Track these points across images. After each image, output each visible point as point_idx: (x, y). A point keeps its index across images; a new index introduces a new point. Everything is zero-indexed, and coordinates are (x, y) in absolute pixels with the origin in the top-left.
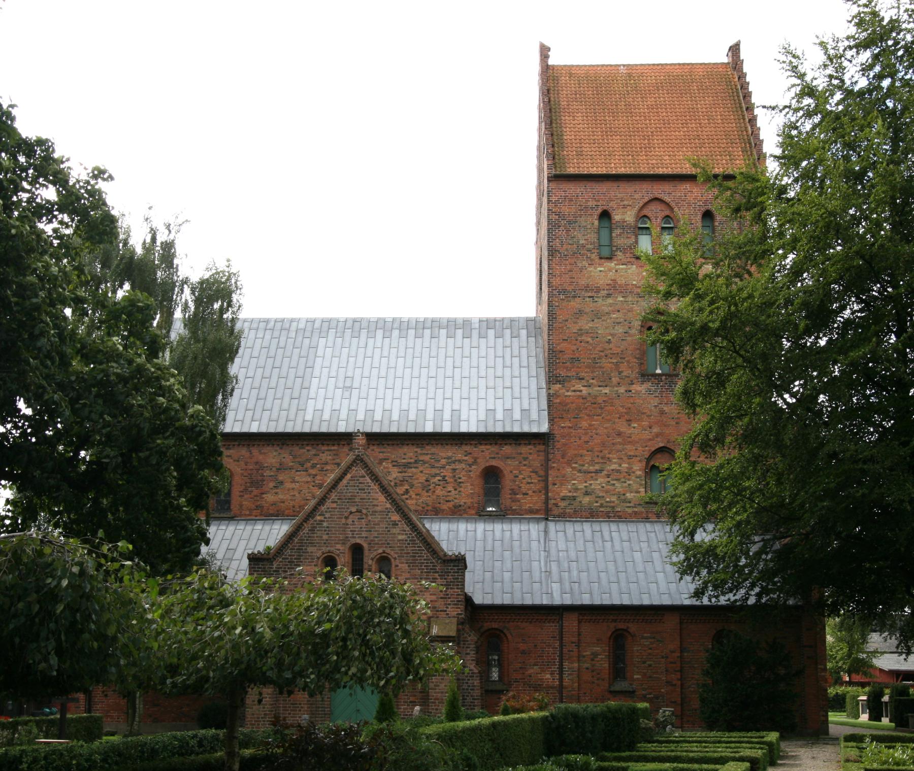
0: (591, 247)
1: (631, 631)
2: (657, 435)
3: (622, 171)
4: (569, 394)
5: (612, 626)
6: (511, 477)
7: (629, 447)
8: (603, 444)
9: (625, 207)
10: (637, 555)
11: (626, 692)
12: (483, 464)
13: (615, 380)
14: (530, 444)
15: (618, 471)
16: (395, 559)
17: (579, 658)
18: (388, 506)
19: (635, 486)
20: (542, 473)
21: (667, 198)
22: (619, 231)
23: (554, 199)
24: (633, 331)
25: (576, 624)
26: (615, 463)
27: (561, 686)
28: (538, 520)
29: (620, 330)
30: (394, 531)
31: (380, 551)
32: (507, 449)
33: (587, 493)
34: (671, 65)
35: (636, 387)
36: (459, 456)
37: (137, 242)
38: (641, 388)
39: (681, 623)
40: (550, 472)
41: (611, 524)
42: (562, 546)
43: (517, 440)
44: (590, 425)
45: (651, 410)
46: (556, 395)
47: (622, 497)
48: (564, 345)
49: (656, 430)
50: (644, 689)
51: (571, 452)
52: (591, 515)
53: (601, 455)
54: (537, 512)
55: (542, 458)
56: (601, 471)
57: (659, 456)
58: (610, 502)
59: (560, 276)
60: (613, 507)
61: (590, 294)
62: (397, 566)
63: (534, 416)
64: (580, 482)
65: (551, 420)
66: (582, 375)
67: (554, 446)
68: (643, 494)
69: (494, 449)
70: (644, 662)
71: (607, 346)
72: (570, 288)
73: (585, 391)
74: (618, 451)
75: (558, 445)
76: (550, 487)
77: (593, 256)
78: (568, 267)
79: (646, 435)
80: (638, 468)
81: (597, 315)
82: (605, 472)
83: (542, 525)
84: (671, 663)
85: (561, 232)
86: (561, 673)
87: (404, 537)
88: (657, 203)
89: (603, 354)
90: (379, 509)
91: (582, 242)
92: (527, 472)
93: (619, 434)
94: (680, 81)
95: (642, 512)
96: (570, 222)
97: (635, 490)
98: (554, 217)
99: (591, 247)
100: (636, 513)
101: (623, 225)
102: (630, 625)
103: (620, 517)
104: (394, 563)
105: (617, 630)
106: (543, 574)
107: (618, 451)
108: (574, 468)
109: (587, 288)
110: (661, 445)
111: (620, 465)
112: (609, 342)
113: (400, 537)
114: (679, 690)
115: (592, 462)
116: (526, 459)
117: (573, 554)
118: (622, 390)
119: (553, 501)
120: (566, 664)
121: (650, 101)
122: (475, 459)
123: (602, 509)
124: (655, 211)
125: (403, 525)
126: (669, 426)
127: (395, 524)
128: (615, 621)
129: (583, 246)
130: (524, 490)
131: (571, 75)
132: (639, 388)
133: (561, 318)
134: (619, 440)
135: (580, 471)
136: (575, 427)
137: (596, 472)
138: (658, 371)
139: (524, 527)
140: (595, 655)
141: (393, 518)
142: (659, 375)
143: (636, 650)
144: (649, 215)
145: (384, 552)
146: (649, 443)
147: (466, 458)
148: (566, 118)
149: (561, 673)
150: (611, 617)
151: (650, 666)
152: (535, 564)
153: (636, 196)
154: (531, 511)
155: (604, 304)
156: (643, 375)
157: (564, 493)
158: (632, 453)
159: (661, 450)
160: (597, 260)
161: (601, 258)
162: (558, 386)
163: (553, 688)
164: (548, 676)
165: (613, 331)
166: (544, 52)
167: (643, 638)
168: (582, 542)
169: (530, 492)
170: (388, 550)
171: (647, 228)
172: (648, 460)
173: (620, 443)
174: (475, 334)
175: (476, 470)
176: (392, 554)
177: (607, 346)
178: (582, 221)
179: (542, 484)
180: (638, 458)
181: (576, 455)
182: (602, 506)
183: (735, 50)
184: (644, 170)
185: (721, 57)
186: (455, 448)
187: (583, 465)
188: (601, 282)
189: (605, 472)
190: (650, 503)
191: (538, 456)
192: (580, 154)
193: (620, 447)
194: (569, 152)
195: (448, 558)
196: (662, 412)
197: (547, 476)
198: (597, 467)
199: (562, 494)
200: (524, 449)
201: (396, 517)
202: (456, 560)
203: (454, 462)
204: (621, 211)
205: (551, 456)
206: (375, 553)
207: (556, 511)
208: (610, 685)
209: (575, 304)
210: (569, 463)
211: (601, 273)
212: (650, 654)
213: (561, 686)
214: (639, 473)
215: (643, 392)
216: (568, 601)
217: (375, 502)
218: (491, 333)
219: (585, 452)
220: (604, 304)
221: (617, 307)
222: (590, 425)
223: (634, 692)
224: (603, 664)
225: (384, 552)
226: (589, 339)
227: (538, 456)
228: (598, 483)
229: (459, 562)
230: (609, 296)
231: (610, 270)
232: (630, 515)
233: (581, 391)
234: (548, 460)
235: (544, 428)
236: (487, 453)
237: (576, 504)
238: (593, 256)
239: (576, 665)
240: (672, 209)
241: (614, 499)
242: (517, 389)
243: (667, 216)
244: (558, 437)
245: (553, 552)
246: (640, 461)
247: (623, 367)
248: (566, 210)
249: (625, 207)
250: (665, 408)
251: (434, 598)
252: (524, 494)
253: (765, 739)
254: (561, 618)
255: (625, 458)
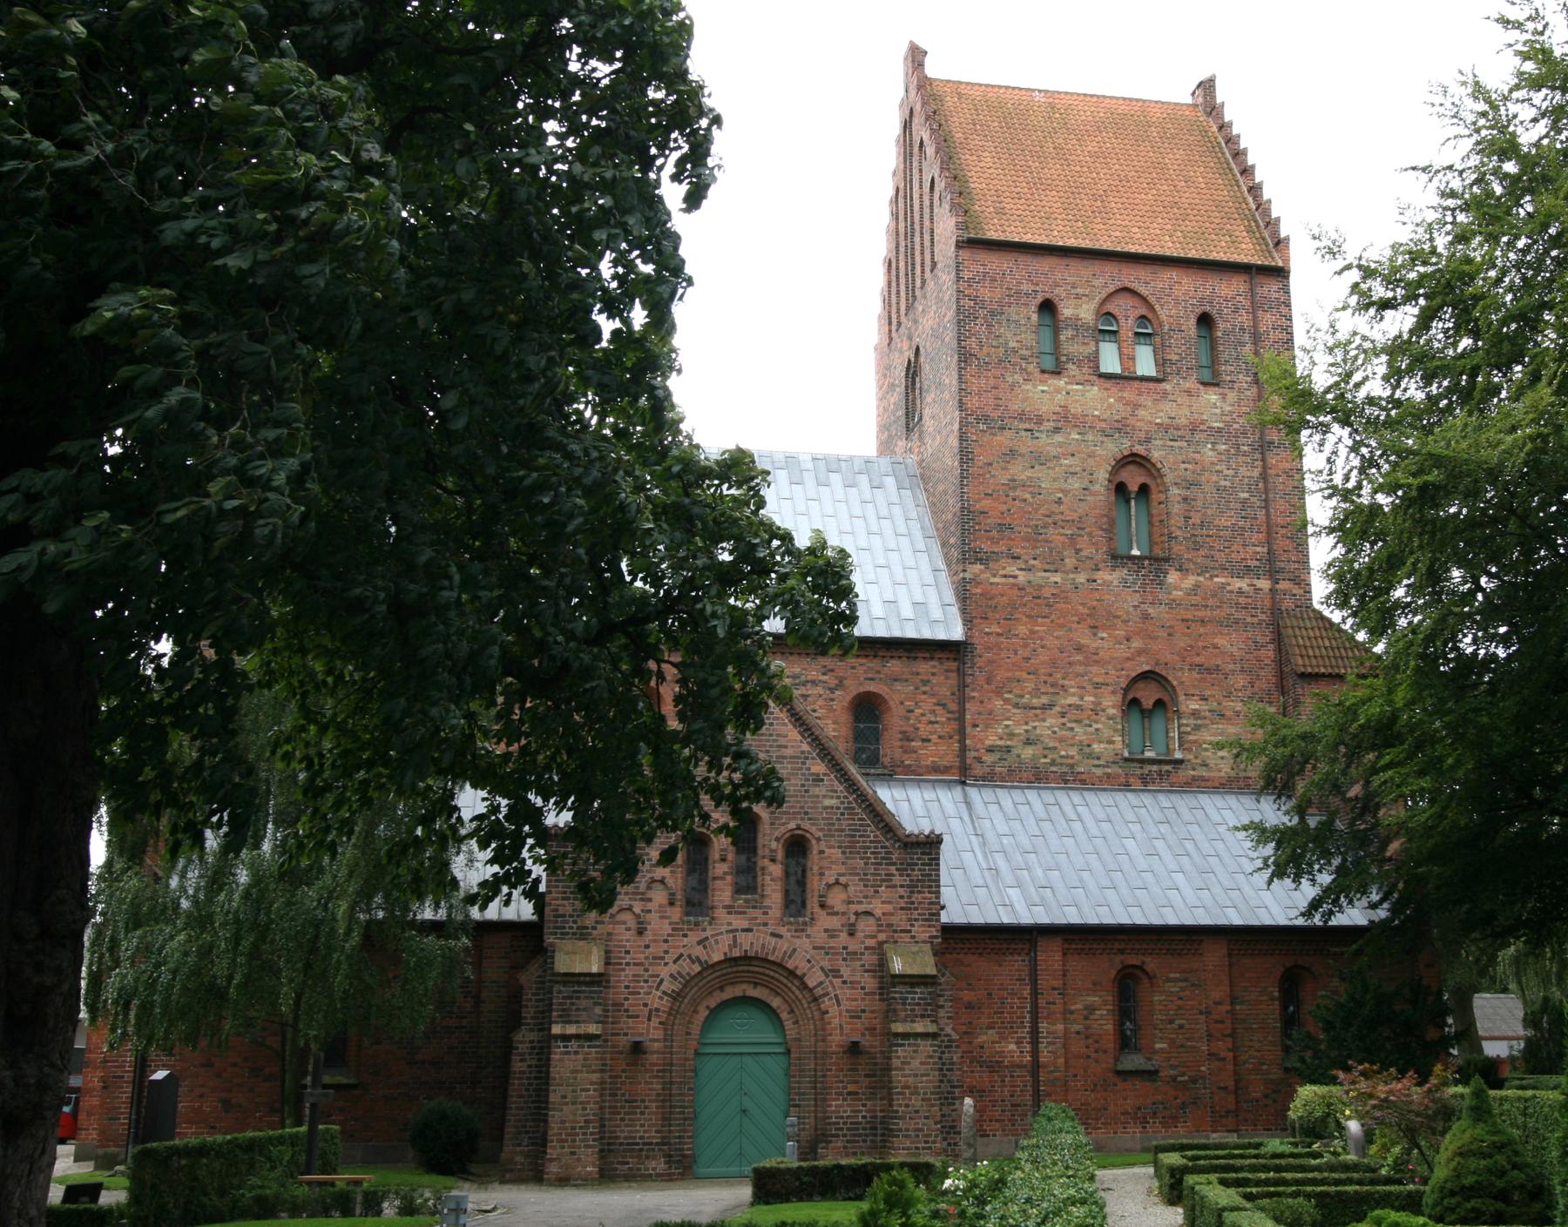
0: (1027, 353)
1: (1148, 968)
2: (1140, 652)
3: (1072, 242)
4: (996, 580)
5: (1118, 961)
6: (901, 711)
7: (1095, 669)
8: (1053, 663)
9: (1078, 297)
10: (1130, 844)
11: (1143, 1072)
12: (854, 688)
13: (1070, 562)
14: (932, 658)
15: (1078, 707)
16: (818, 840)
17: (1067, 1014)
18: (805, 747)
19: (1106, 733)
20: (953, 706)
21: (1143, 290)
22: (1069, 333)
23: (966, 275)
24: (1097, 487)
25: (1058, 956)
26: (1074, 694)
27: (1036, 1066)
28: (949, 784)
29: (1075, 484)
30: (816, 791)
31: (792, 825)
32: (895, 666)
33: (1028, 742)
34: (1111, 98)
35: (1104, 576)
36: (813, 674)
37: (1265, 197)
38: (1111, 576)
39: (1230, 955)
40: (967, 706)
41: (1071, 793)
42: (1002, 827)
43: (910, 651)
44: (1032, 632)
45: (1128, 613)
46: (974, 581)
47: (1086, 750)
48: (986, 503)
49: (1136, 644)
50: (1173, 1067)
51: (1001, 675)
52: (1038, 777)
53: (1050, 680)
54: (946, 770)
55: (955, 682)
56: (1051, 706)
57: (1141, 685)
58: (1067, 757)
59: (979, 394)
60: (1072, 766)
61: (1027, 426)
62: (822, 852)
63: (937, 613)
64: (1018, 723)
65: (968, 622)
66: (1017, 551)
67: (974, 664)
68: (1119, 745)
69: (873, 664)
70: (1171, 1022)
71: (1055, 508)
72: (995, 415)
73: (1022, 577)
74: (1077, 675)
75: (980, 662)
76: (969, 730)
77: (1031, 368)
78: (992, 382)
79: (1122, 651)
80: (1111, 704)
81: (1039, 459)
82: (1058, 709)
83: (958, 791)
84: (1217, 1022)
85: (980, 327)
86: (1035, 1041)
87: (833, 802)
88: (1128, 295)
89: (1050, 520)
90: (788, 752)
91: (1011, 344)
92: (927, 704)
93: (1079, 648)
94: (1129, 121)
95: (1119, 776)
96: (992, 313)
97: (1108, 737)
98: (967, 303)
99: (1027, 353)
100: (1109, 776)
101: (1076, 324)
102: (1148, 959)
103: (1083, 782)
104: (815, 848)
105: (1125, 967)
106: (986, 873)
107: (1077, 675)
108: (1006, 701)
109: (1021, 416)
110: (1147, 668)
111: (1082, 699)
112: (1059, 502)
113: (827, 802)
114: (1230, 1067)
115: (1036, 692)
116: (925, 682)
117: (1025, 842)
118: (1081, 578)
119: (973, 754)
120: (1043, 1026)
121: (1092, 146)
122: (841, 680)
123: (1054, 769)
124: (1121, 306)
125: (831, 781)
126: (1156, 638)
127: (818, 780)
128: (1121, 951)
129: (1015, 351)
130: (923, 734)
131: (960, 96)
132: (1108, 577)
133: (981, 460)
134: (1080, 657)
135: (1016, 706)
136: (1007, 634)
137: (1043, 708)
138: (1135, 552)
139: (929, 794)
140: (1091, 1009)
141: (815, 769)
142: (1135, 557)
143: (1159, 1000)
144: (1115, 312)
145: (799, 828)
146: (1128, 665)
147: (825, 678)
148: (966, 158)
149: (1035, 1041)
150: (1116, 945)
151: (1181, 1027)
152: (967, 856)
153: (1096, 282)
154: (936, 769)
155: (1048, 443)
156: (1114, 557)
157: (992, 740)
158: (1099, 680)
159: (1145, 676)
160: (1037, 375)
161: (1043, 372)
162: (979, 567)
163: (1020, 1066)
164: (1013, 1047)
165: (1064, 486)
166: (916, 57)
167: (1169, 980)
168: (1033, 822)
169: (934, 737)
170: (806, 825)
171: (1114, 332)
172: (1126, 690)
173: (1081, 663)
174: (809, 478)
175: (843, 699)
176: (813, 830)
177: (1055, 508)
178: (1012, 312)
179: (955, 725)
180: (1110, 688)
181: (1009, 680)
182: (1053, 763)
183: (1207, 87)
184: (1105, 244)
185: (1181, 93)
186: (805, 661)
187: (1022, 696)
188: (1045, 409)
189: (1058, 709)
190: (1132, 760)
191: (947, 678)
192: (1001, 212)
193: (1080, 669)
194: (983, 208)
195: (913, 839)
196: (1146, 617)
197: (962, 711)
198: (1044, 700)
199: (988, 743)
200: (924, 667)
201: (819, 768)
202: (925, 844)
203: (804, 684)
204: (1072, 302)
205: (969, 680)
206: (782, 829)
207: (978, 770)
208: (1116, 1059)
209: (1004, 439)
210: (998, 693)
211: (1044, 394)
212: (1180, 1008)
213: (1036, 1066)
214: (1112, 711)
215: (1116, 583)
216: (1043, 918)
217: (782, 741)
218: (836, 478)
219: (1025, 675)
220: (1048, 443)
221: (1071, 449)
222: (1032, 632)
223: (1156, 1072)
224: (1105, 1023)
225: (799, 828)
226: (1028, 496)
227: (947, 678)
228: (1046, 726)
229: (930, 845)
230: (1057, 430)
231: (1058, 391)
232: (1100, 779)
233: (1015, 577)
234: (963, 686)
235: (955, 631)
236: (860, 670)
237: (1011, 758)
238: (1031, 368)
239: (1060, 1027)
240: (1151, 308)
241: (1073, 752)
242: (898, 570)
243: (1143, 317)
244: (979, 649)
245: (990, 835)
246: (1113, 692)
247: (1083, 542)
248: (986, 293)
249: (1078, 297)
250: (1151, 611)
251: (889, 908)
252: (924, 740)
253: (1263, 1150)
254: (1034, 947)
255: (1089, 688)
